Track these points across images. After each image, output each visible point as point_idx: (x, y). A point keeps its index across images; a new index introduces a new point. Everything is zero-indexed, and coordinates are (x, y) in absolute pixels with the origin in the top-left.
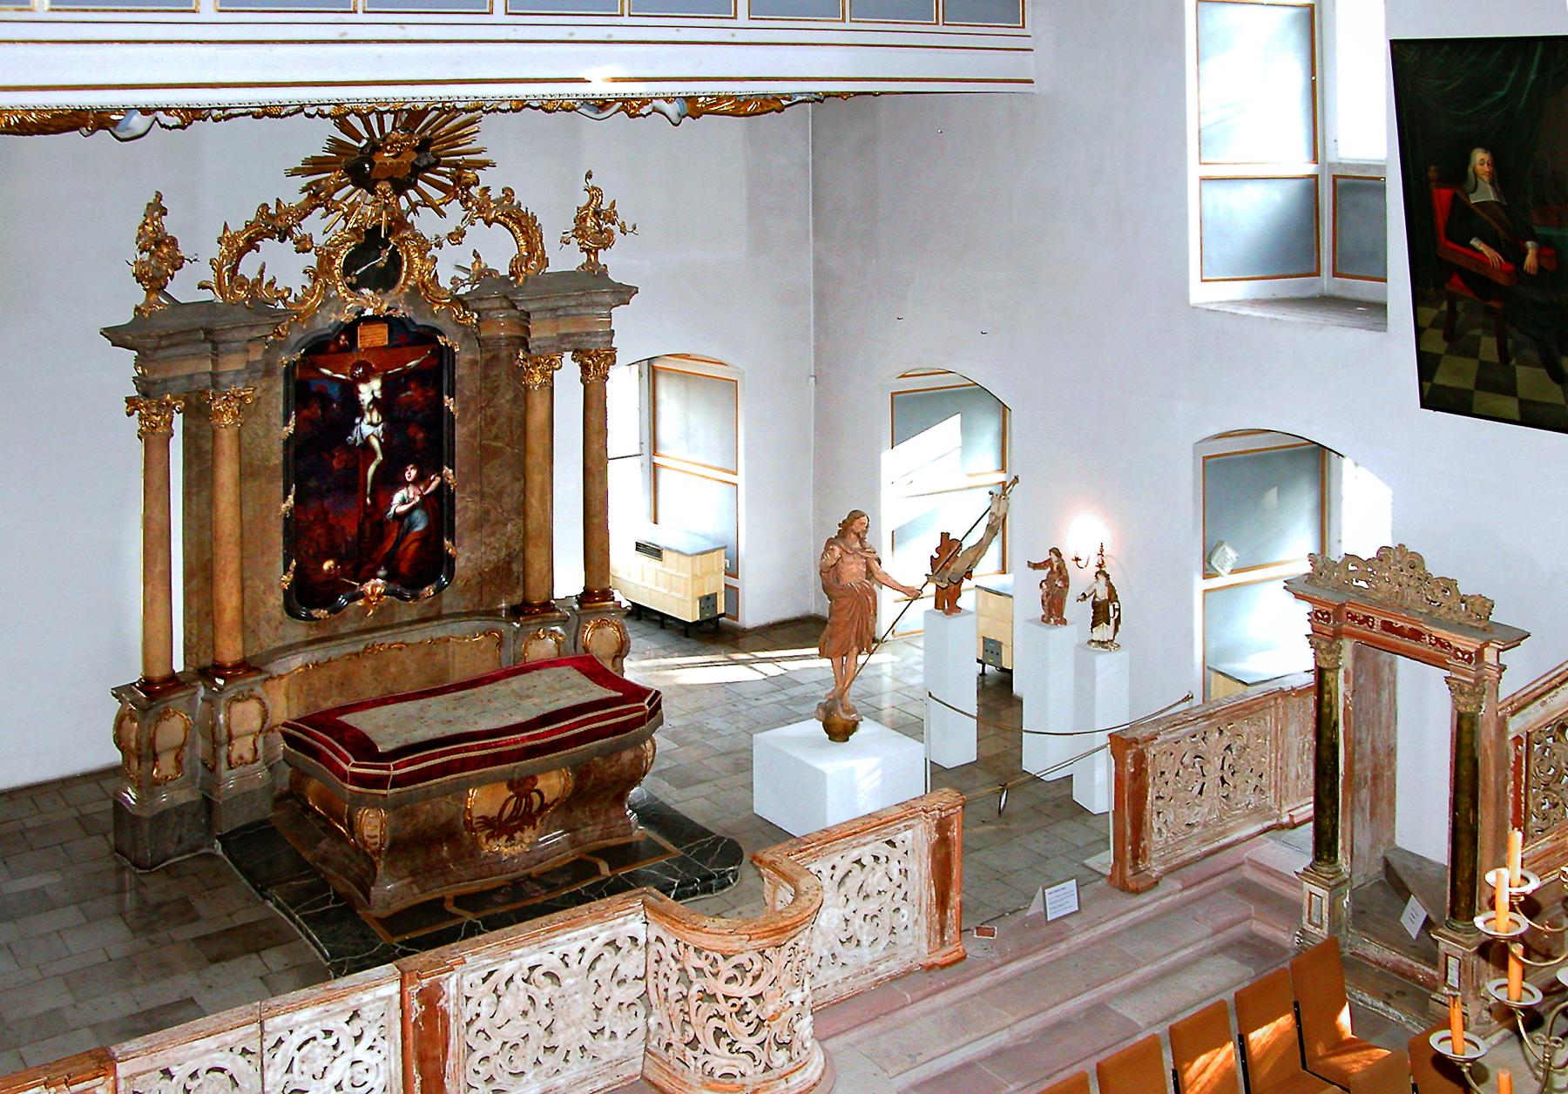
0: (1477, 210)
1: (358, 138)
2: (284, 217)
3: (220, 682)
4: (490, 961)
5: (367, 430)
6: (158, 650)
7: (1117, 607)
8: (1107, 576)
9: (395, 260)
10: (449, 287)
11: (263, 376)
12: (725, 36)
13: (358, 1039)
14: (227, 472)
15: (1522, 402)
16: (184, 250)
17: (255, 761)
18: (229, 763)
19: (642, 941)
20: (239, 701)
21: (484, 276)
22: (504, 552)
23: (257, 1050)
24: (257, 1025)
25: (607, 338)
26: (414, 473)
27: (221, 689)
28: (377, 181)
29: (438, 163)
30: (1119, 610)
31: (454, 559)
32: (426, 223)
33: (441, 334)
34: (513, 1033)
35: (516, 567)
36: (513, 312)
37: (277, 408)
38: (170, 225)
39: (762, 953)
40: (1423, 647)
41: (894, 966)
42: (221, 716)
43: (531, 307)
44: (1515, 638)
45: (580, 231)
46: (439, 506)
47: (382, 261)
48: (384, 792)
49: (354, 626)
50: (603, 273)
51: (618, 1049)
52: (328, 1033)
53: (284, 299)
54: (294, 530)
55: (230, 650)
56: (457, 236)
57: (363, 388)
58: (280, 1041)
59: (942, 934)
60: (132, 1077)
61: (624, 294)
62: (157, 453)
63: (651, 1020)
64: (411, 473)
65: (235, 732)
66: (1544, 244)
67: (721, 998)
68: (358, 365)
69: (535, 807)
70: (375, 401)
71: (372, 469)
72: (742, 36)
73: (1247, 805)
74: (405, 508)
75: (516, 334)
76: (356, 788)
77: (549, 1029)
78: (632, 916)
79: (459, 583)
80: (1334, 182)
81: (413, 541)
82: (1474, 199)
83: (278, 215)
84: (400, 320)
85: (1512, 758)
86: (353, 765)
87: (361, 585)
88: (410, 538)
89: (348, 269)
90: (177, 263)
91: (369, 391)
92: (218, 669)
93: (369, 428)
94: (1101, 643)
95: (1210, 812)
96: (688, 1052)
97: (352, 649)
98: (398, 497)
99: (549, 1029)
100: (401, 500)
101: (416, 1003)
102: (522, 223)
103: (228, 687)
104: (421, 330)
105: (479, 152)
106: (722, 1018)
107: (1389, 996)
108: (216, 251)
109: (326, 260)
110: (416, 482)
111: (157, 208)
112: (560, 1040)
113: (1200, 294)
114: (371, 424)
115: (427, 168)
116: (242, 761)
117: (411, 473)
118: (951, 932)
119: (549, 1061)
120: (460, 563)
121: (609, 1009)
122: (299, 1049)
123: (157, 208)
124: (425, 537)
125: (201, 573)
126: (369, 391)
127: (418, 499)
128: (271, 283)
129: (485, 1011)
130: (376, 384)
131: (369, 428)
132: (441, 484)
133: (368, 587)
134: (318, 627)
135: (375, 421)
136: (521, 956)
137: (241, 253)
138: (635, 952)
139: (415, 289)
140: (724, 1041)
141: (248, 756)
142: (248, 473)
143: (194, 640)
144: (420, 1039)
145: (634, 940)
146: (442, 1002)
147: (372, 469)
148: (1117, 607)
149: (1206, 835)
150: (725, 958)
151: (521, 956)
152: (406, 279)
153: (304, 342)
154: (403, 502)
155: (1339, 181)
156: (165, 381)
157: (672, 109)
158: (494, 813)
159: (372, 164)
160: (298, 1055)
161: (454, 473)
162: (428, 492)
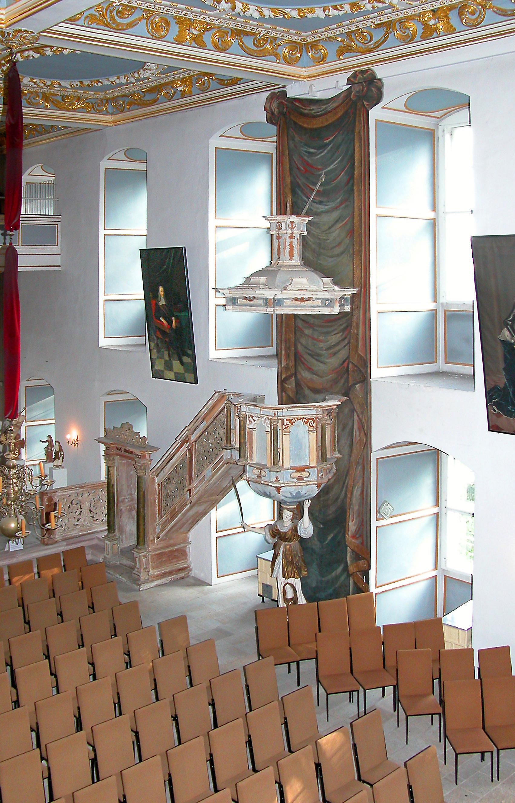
0: (162, 308)
7: (62, 453)
8: (59, 443)
15: (175, 373)
30: (63, 454)
44: (156, 449)
66: (177, 318)
73: (102, 521)
80: (445, 313)
82: (161, 304)
85: (157, 491)
94: (57, 466)
95: (84, 521)
107: (122, 574)
113: (103, 342)
148: (62, 453)
149: (83, 529)
155: (447, 313)
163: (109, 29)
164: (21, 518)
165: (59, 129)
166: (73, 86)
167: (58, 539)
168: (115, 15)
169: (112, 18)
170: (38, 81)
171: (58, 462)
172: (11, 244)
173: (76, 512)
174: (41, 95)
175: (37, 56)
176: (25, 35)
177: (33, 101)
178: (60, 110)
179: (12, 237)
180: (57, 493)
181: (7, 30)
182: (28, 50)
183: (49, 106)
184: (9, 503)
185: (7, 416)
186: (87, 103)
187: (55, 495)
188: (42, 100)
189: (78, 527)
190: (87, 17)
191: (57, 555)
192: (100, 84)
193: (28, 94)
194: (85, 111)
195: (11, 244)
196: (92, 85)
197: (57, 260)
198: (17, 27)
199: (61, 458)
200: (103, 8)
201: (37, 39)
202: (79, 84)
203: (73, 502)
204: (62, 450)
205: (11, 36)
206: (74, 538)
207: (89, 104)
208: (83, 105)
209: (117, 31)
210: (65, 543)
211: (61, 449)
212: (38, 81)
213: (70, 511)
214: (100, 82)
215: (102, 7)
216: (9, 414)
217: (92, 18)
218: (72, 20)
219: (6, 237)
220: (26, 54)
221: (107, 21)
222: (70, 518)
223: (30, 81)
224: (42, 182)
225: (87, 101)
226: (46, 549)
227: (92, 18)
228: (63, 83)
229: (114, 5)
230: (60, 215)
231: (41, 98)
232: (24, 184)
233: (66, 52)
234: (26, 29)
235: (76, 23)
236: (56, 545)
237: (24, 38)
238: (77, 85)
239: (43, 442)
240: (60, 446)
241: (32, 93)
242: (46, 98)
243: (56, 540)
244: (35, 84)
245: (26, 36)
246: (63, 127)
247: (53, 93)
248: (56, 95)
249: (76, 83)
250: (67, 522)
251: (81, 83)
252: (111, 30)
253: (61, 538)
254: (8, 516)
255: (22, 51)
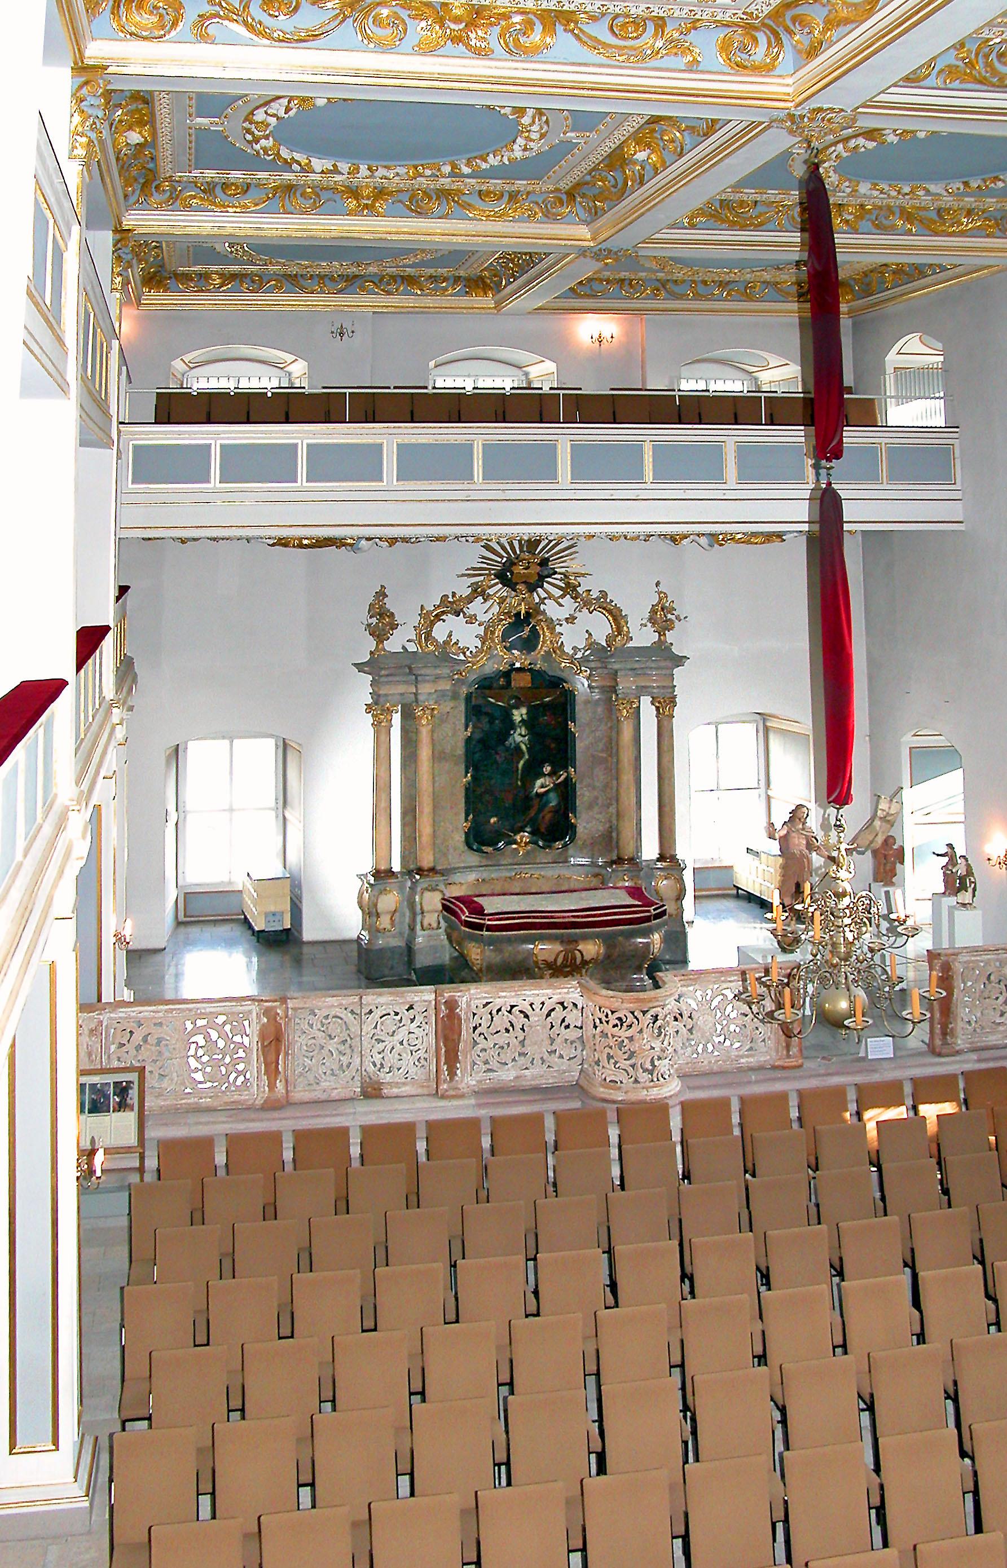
1: (502, 557)
2: (458, 603)
3: (418, 877)
4: (487, 995)
5: (518, 739)
6: (383, 853)
9: (535, 634)
10: (571, 652)
11: (450, 700)
12: (719, 495)
13: (412, 1021)
14: (425, 753)
16: (399, 619)
17: (439, 928)
18: (422, 926)
19: (580, 1006)
20: (429, 891)
21: (591, 645)
22: (608, 825)
23: (359, 1012)
24: (357, 998)
25: (670, 690)
26: (549, 768)
27: (417, 881)
28: (517, 584)
29: (555, 573)
31: (576, 827)
32: (551, 609)
33: (566, 682)
34: (503, 1039)
35: (614, 835)
36: (606, 671)
37: (460, 720)
38: (390, 604)
39: (633, 1013)
40: (614, 735)
41: (752, 1061)
42: (417, 897)
43: (616, 666)
45: (652, 620)
46: (567, 791)
47: (526, 632)
48: (481, 933)
49: (510, 861)
50: (668, 648)
51: (564, 1065)
52: (397, 1014)
53: (464, 654)
54: (471, 794)
55: (427, 860)
56: (571, 620)
57: (515, 712)
58: (371, 1012)
59: (788, 1051)
60: (294, 1009)
61: (679, 661)
62: (383, 737)
63: (584, 1053)
64: (547, 769)
65: (425, 908)
67: (609, 1035)
68: (511, 698)
69: (579, 961)
70: (523, 721)
71: (522, 763)
72: (730, 495)
74: (543, 790)
75: (608, 684)
76: (467, 930)
77: (522, 1043)
78: (572, 990)
79: (580, 843)
81: (550, 812)
83: (454, 602)
84: (538, 671)
86: (467, 917)
87: (515, 835)
88: (547, 809)
89: (504, 637)
90: (394, 626)
91: (519, 714)
92: (420, 871)
93: (519, 737)
94: (964, 905)
96: (596, 1067)
97: (508, 874)
98: (539, 783)
99: (522, 1043)
100: (540, 785)
101: (443, 1007)
102: (616, 617)
103: (422, 880)
104: (553, 679)
105: (483, 557)
106: (611, 1048)
108: (415, 620)
109: (489, 628)
110: (550, 775)
111: (381, 594)
112: (528, 1049)
114: (520, 734)
115: (549, 576)
116: (430, 927)
117: (547, 769)
118: (794, 1050)
119: (521, 1061)
120: (580, 829)
121: (559, 1040)
122: (381, 1018)
123: (381, 594)
124: (556, 811)
125: (410, 812)
126: (519, 714)
127: (552, 785)
128: (456, 643)
129: (484, 1025)
130: (524, 711)
131: (519, 737)
132: (566, 779)
133: (518, 838)
134: (487, 858)
135: (523, 733)
136: (505, 997)
137: (432, 624)
138: (575, 1011)
139: (548, 653)
140: (612, 1061)
141: (435, 925)
142: (438, 756)
143: (407, 852)
144: (444, 1028)
145: (575, 1005)
146: (458, 1010)
147: (522, 763)
150: (613, 1012)
151: (505, 997)
152: (542, 646)
153: (478, 680)
154: (542, 787)
156: (386, 695)
157: (703, 541)
158: (551, 959)
159: (512, 574)
160: (380, 1021)
161: (575, 771)
162: (559, 781)
163: (985, 88)
164: (860, 993)
165: (943, 269)
166: (950, 191)
167: (962, 1046)
168: (995, 60)
169: (989, 65)
170: (887, 188)
171: (966, 897)
172: (829, 484)
173: (997, 998)
174: (897, 211)
175: (871, 145)
176: (831, 115)
177: (884, 222)
178: (936, 234)
179: (831, 472)
180: (960, 957)
181: (798, 111)
182: (856, 136)
183: (914, 230)
184: (835, 962)
185: (831, 799)
186: (986, 219)
187: (955, 960)
188: (900, 219)
189: (1001, 1028)
190: (941, 71)
191: (952, 1078)
192: (1000, 184)
193: (873, 211)
194: (983, 233)
195: (829, 484)
196: (987, 187)
197: (955, 511)
198: (814, 104)
199: (970, 890)
200: (969, 51)
201: (854, 120)
202: (962, 187)
203: (992, 977)
204: (972, 874)
205: (806, 120)
206: (992, 1049)
207: (990, 221)
208: (978, 224)
209: (1001, 90)
210: (974, 1056)
211: (969, 872)
212: (887, 188)
213: (986, 994)
214: (1000, 180)
215: (968, 50)
216: (836, 794)
217: (951, 72)
218: (912, 80)
219: (820, 471)
220: (852, 143)
221: (979, 73)
222: (986, 1008)
223: (870, 189)
224: (920, 365)
225: (985, 215)
226: (937, 1064)
227: (951, 72)
228: (932, 188)
229: (991, 43)
230: (957, 427)
231: (898, 215)
232: (890, 370)
233: (921, 135)
234: (831, 106)
235: (922, 84)
236: (958, 1058)
237: (829, 120)
238: (958, 189)
239: (938, 855)
240: (968, 866)
241: (880, 208)
242: (908, 216)
243: (958, 1048)
244: (882, 193)
245: (832, 118)
246: (951, 265)
247: (918, 205)
248: (926, 209)
249: (957, 185)
250: (979, 1015)
251: (966, 184)
252: (990, 89)
253: (967, 1045)
254: (834, 987)
255: (846, 140)
